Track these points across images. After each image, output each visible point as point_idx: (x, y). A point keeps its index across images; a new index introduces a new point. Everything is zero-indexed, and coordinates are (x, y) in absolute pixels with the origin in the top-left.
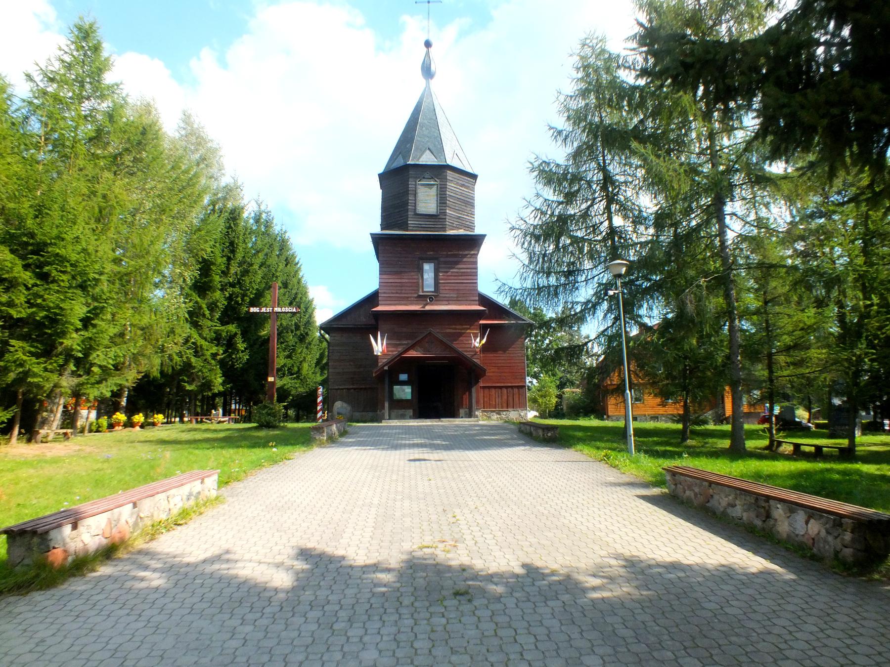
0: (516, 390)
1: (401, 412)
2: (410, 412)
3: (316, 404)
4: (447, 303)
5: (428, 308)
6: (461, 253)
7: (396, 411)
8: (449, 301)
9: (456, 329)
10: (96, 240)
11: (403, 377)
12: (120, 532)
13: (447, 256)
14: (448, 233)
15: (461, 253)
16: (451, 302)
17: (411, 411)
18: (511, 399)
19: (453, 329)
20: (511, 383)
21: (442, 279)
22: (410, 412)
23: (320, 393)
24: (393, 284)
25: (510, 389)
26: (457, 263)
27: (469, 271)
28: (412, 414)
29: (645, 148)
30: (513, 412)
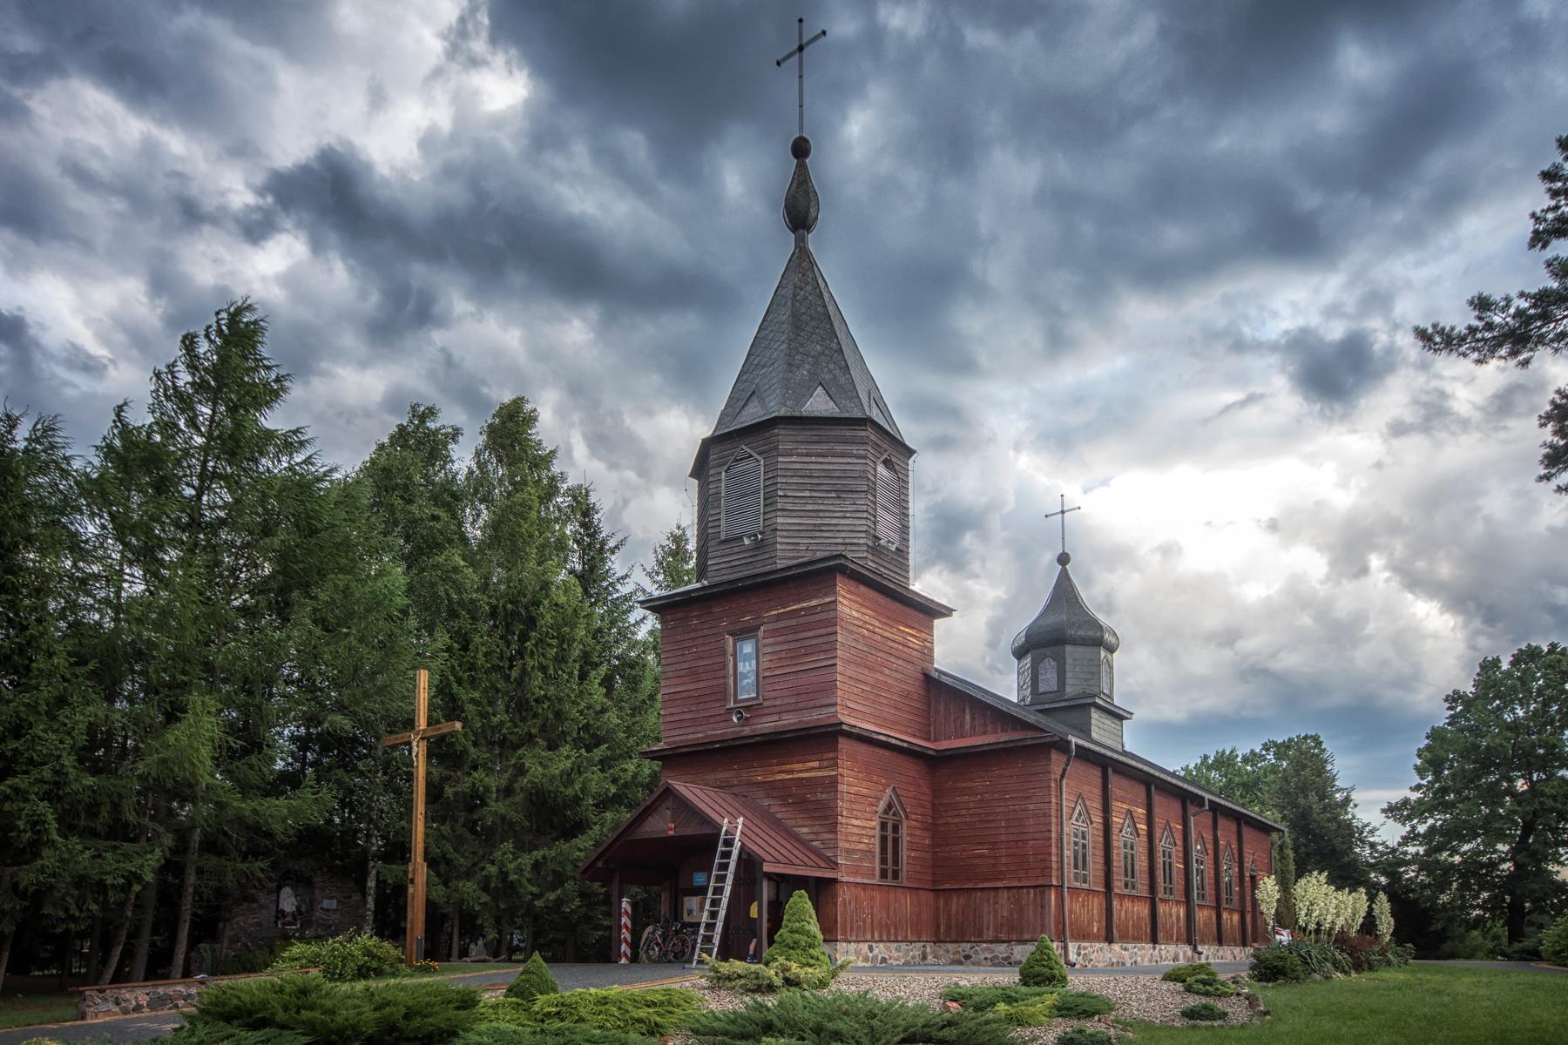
9: (792, 772)
27: (820, 640)
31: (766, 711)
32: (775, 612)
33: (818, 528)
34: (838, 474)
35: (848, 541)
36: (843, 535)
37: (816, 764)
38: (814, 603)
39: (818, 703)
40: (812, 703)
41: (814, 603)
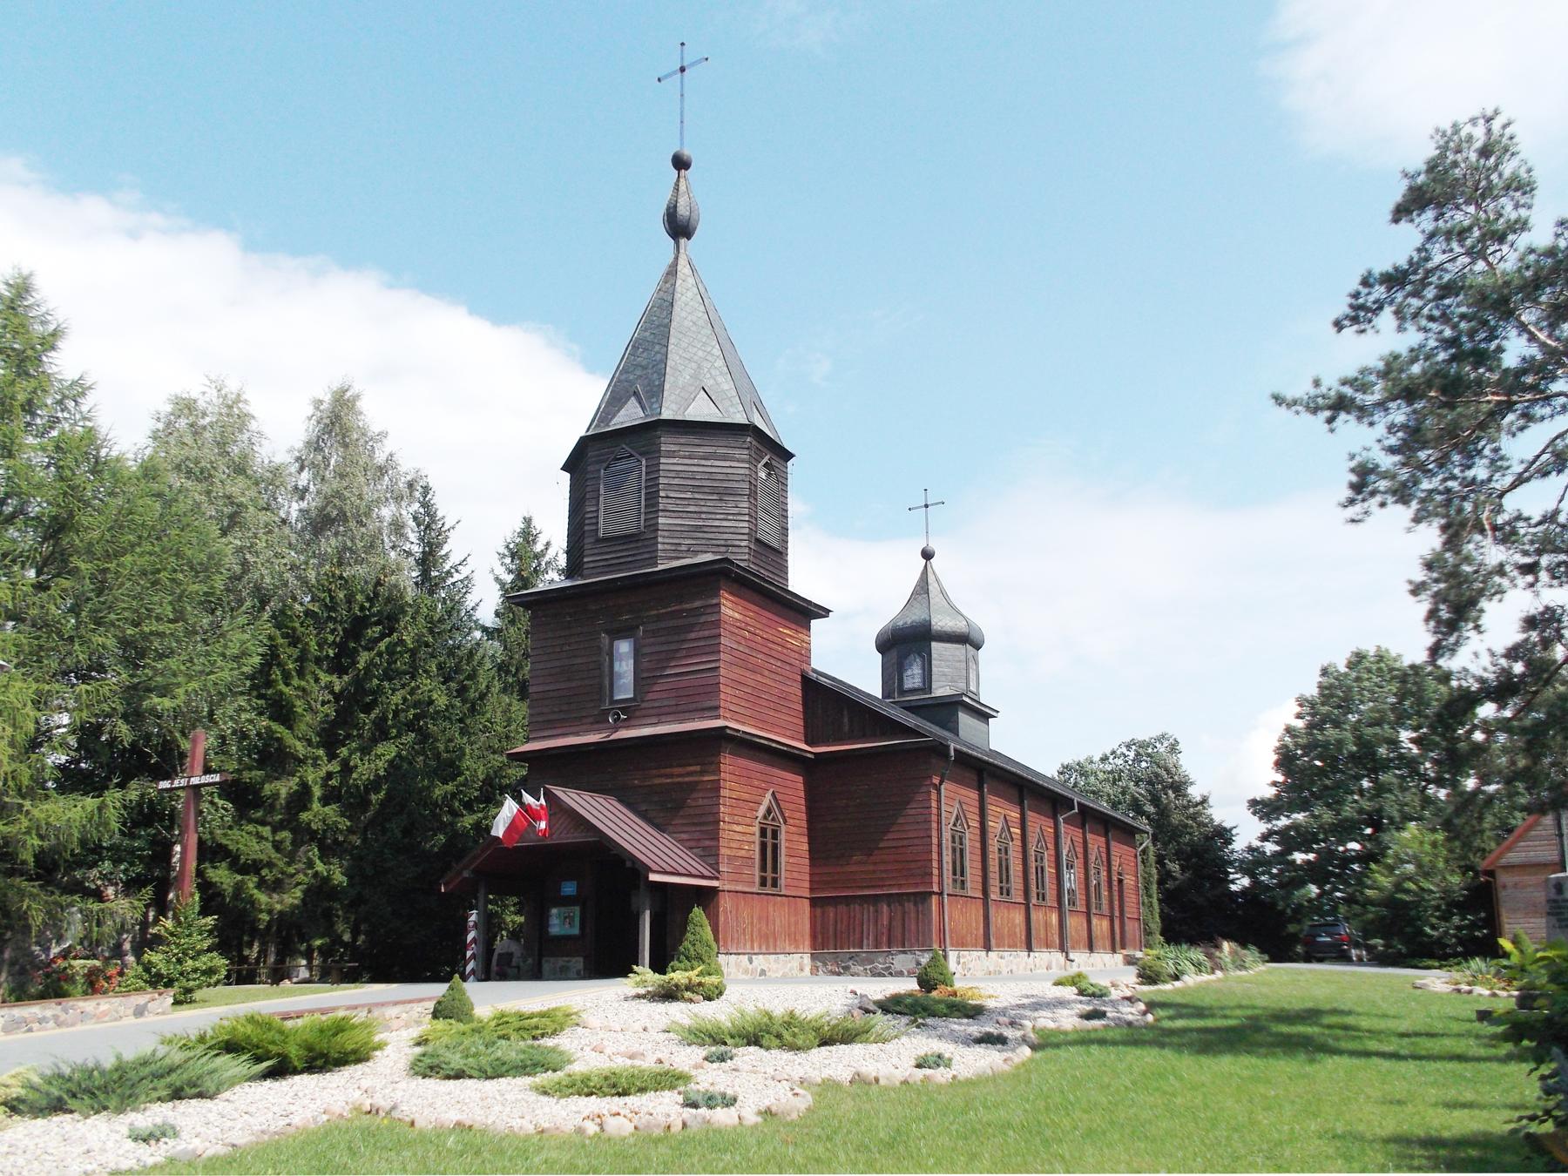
0: (910, 906)
1: (561, 961)
2: (578, 963)
3: (465, 947)
4: (654, 720)
5: (614, 736)
6: (687, 606)
7: (552, 959)
8: (661, 715)
9: (672, 776)
10: (451, 740)
11: (569, 888)
12: (570, 1076)
13: (659, 618)
14: (660, 568)
15: (687, 606)
16: (663, 718)
17: (581, 959)
18: (897, 924)
19: (667, 776)
20: (900, 886)
21: (648, 670)
22: (578, 963)
23: (471, 924)
24: (551, 694)
25: (842, 908)
26: (690, 628)
28: (580, 965)
29: (1383, 729)
30: (902, 956)
31: (644, 712)
32: (654, 612)
33: (698, 529)
34: (721, 477)
35: (729, 543)
36: (725, 536)
37: (698, 768)
38: (697, 604)
39: (699, 706)
40: (694, 706)
41: (697, 604)
